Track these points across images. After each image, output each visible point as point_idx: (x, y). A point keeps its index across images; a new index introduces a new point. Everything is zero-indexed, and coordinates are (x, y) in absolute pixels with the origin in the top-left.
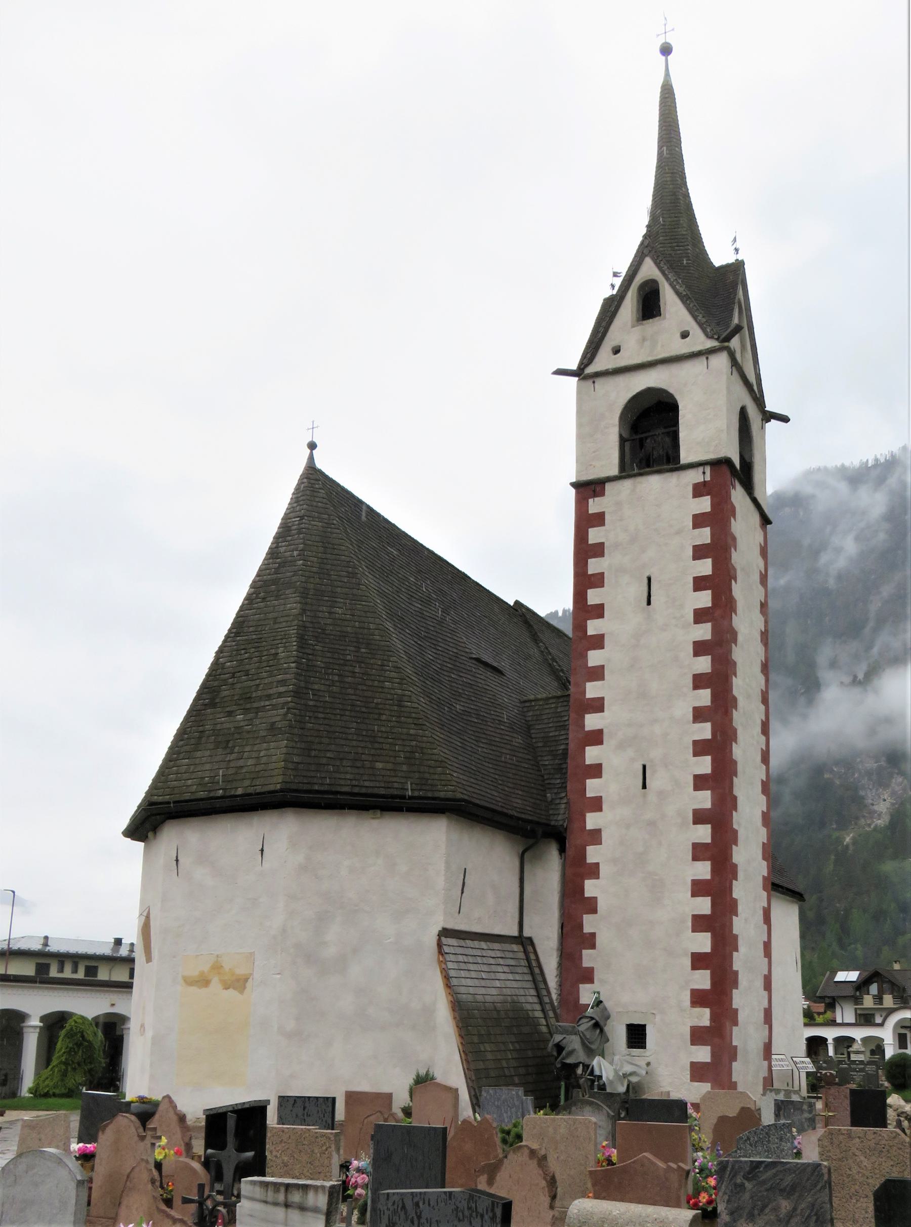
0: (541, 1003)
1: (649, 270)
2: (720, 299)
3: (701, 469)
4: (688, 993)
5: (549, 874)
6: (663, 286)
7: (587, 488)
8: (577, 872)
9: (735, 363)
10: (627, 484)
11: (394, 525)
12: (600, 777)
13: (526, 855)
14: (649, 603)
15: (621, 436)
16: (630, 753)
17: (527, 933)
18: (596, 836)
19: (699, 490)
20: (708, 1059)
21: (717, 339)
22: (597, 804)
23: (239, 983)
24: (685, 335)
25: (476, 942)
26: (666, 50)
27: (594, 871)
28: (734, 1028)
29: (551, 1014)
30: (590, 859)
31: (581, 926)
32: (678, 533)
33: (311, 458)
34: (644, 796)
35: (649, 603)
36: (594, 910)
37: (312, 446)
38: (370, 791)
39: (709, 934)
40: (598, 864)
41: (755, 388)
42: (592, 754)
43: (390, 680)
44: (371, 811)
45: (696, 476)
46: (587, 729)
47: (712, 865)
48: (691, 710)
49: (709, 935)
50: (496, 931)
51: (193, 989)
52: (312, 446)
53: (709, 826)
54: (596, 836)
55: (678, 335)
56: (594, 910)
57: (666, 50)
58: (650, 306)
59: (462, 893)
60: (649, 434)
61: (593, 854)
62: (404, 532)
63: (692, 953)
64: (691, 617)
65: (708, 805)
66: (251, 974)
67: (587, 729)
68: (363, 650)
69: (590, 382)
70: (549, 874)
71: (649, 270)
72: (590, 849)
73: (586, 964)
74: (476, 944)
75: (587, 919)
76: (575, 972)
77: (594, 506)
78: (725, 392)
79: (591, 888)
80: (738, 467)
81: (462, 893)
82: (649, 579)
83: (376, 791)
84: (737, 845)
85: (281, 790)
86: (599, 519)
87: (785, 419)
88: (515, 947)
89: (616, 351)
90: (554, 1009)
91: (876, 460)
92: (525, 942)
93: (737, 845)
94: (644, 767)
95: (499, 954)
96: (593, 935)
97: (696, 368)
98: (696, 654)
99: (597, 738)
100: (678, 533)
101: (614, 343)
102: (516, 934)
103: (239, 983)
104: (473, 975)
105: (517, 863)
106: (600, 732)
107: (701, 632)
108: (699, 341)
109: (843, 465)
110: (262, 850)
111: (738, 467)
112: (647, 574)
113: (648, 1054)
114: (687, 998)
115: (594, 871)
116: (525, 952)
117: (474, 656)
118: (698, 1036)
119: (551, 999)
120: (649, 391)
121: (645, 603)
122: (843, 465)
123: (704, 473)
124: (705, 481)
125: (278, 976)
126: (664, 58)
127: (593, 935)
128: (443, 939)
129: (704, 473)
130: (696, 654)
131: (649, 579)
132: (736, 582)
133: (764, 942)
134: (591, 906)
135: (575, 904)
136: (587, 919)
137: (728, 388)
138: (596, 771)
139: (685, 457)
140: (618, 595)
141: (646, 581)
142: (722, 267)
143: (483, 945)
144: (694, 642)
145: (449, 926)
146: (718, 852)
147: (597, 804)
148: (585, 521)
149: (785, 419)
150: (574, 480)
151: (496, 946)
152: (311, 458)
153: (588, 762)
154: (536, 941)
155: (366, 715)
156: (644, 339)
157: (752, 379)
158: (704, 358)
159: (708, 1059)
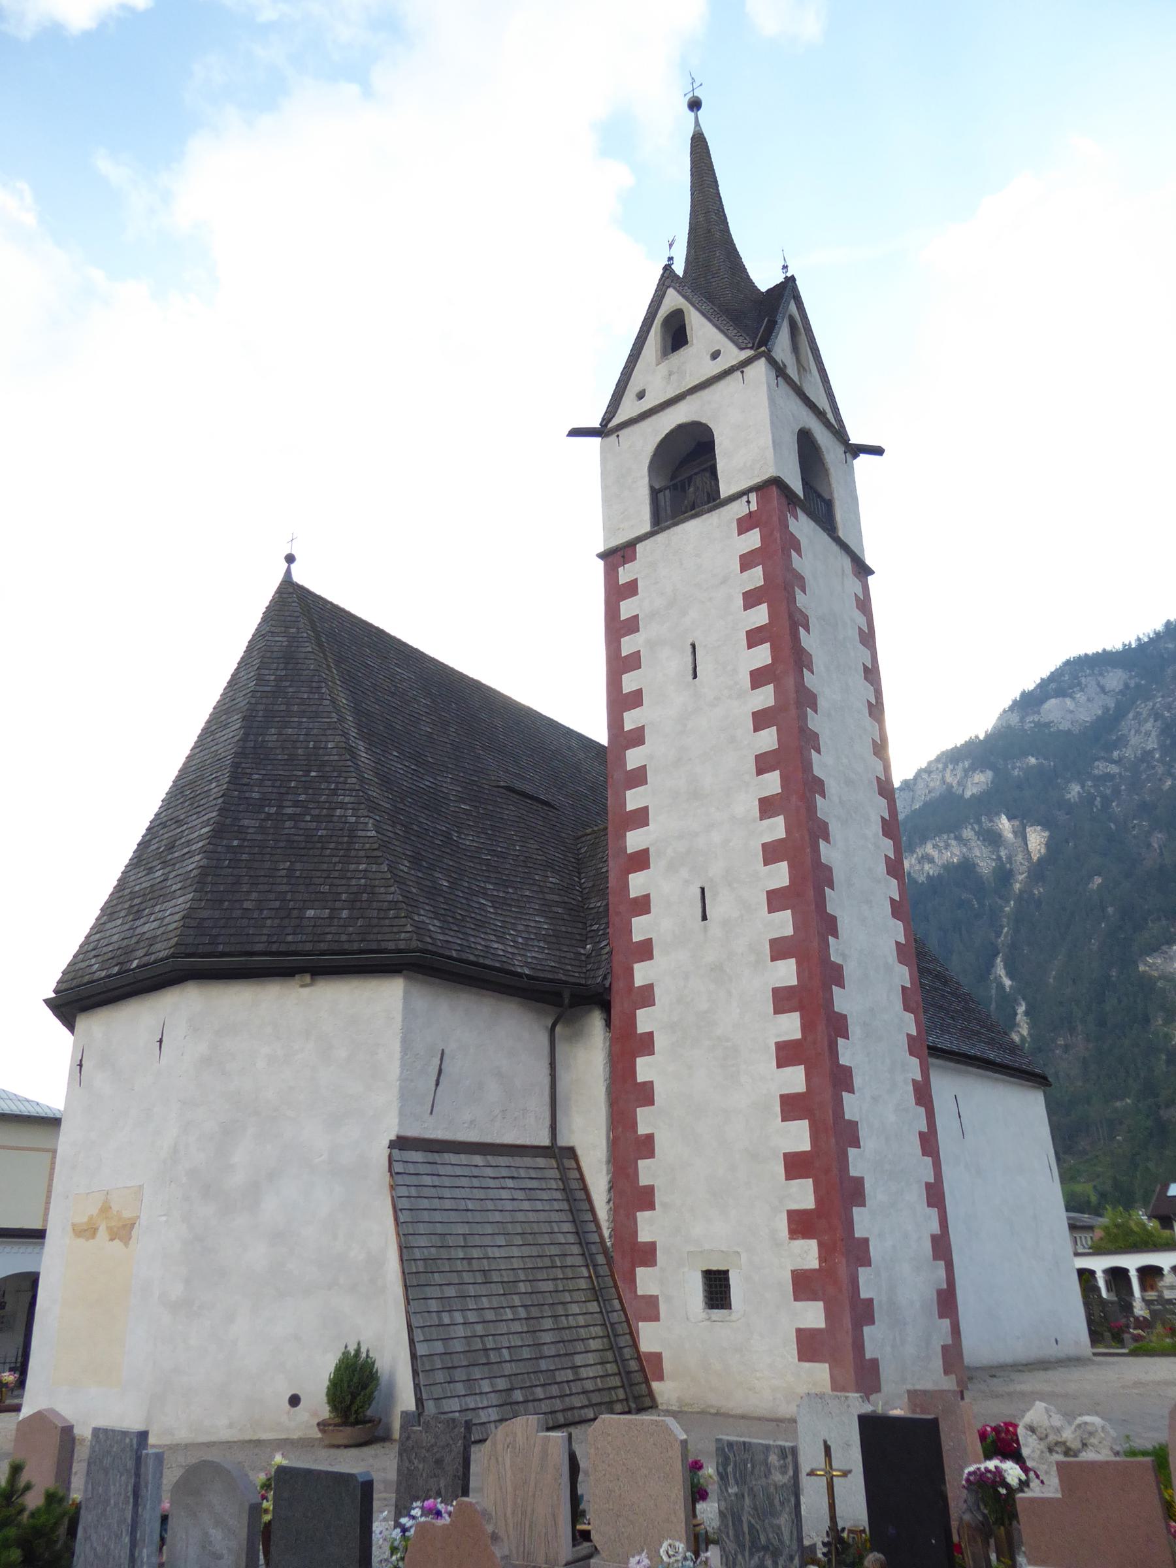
0: (583, 1243)
1: (673, 300)
2: (765, 319)
3: (745, 498)
4: (785, 1216)
5: (589, 1057)
6: (689, 312)
7: (617, 556)
8: (629, 1046)
9: (780, 371)
10: (660, 538)
11: (417, 650)
12: (649, 912)
13: (558, 1029)
14: (695, 676)
15: (652, 489)
16: (684, 873)
17: (562, 1142)
18: (646, 996)
19: (744, 525)
20: (821, 1324)
21: (751, 348)
22: (645, 950)
23: (124, 1231)
24: (715, 355)
25: (462, 1156)
26: (695, 105)
27: (646, 1044)
28: (862, 1271)
29: (601, 1259)
30: (642, 1027)
31: (634, 1125)
32: (724, 581)
33: (288, 573)
34: (705, 930)
35: (695, 676)
36: (649, 1100)
37: (290, 559)
38: (293, 948)
39: (806, 1122)
40: (651, 1033)
41: (830, 416)
42: (638, 883)
43: (343, 806)
44: (297, 977)
45: (739, 509)
46: (629, 852)
47: (802, 1018)
48: (757, 803)
49: (805, 1123)
50: (509, 1138)
51: (80, 1242)
52: (290, 559)
53: (793, 960)
54: (646, 996)
55: (709, 357)
56: (649, 1100)
57: (695, 105)
58: (676, 336)
59: (437, 1084)
60: (684, 475)
61: (645, 1020)
62: (377, 629)
63: (785, 1155)
64: (747, 681)
65: (789, 931)
66: (138, 1217)
67: (629, 852)
68: (313, 774)
69: (614, 437)
70: (589, 1057)
71: (673, 300)
72: (641, 1014)
73: (643, 1181)
74: (463, 1158)
75: (642, 1113)
76: (634, 1197)
77: (625, 575)
78: (766, 403)
79: (645, 1069)
80: (801, 495)
81: (437, 1084)
82: (693, 646)
83: (300, 947)
84: (842, 985)
85: (173, 956)
86: (632, 588)
87: (877, 451)
88: (541, 1162)
89: (641, 395)
90: (605, 1252)
91: (1139, 639)
92: (563, 1156)
93: (842, 985)
94: (703, 890)
95: (505, 1172)
96: (650, 1138)
97: (732, 384)
98: (757, 728)
99: (641, 860)
100: (724, 581)
101: (638, 389)
102: (546, 1142)
103: (124, 1231)
104: (448, 1204)
105: (543, 1039)
106: (646, 852)
107: (762, 697)
108: (733, 355)
109: (1104, 650)
110: (161, 1041)
111: (801, 495)
112: (690, 641)
113: (734, 1316)
114: (782, 1225)
115: (646, 1044)
116: (561, 1169)
117: (502, 784)
118: (804, 1285)
119: (601, 1236)
120: (681, 428)
121: (691, 677)
122: (1104, 650)
123: (748, 502)
124: (750, 512)
125: (164, 1218)
126: (692, 115)
127: (650, 1138)
128: (396, 1152)
129: (748, 502)
130: (757, 728)
131: (693, 646)
132: (808, 631)
133: (921, 1134)
134: (645, 1094)
135: (627, 1094)
136: (642, 1113)
137: (772, 400)
138: (643, 905)
139: (725, 491)
140: (658, 675)
141: (690, 649)
142: (769, 290)
143: (478, 1160)
144: (754, 714)
145: (413, 1132)
146: (814, 998)
147: (645, 950)
148: (618, 592)
149: (877, 451)
150: (601, 549)
151: (503, 1161)
152: (288, 573)
153: (633, 894)
154: (579, 1152)
155: (303, 852)
156: (670, 374)
157: (823, 403)
158: (739, 373)
159: (821, 1324)
